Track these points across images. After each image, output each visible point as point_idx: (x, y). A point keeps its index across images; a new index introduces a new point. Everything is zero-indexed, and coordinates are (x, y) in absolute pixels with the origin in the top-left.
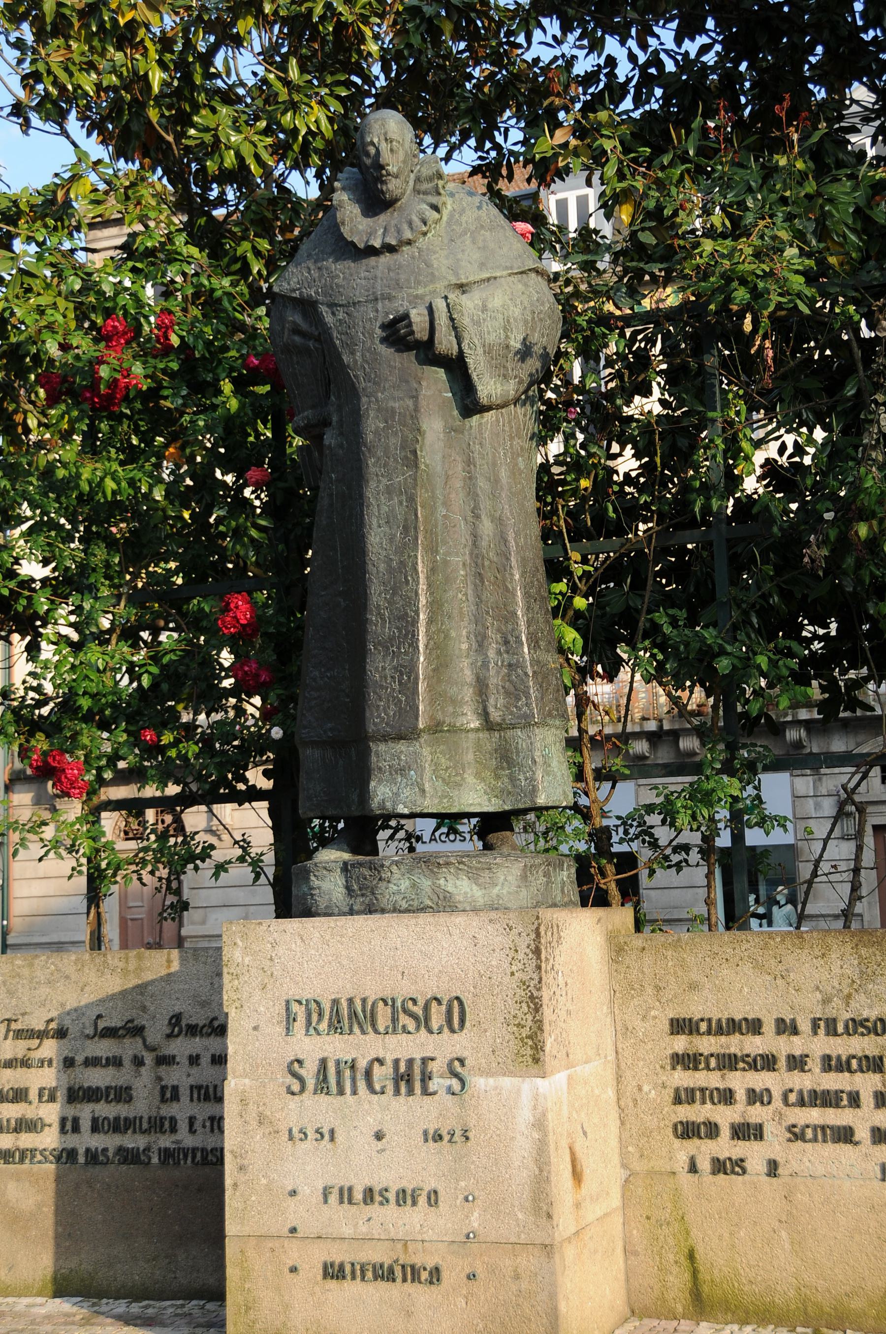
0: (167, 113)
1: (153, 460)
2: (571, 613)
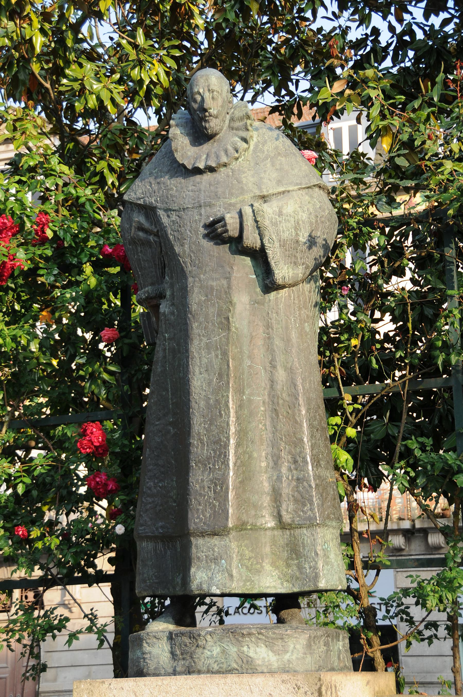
0: (46, 67)
1: (31, 321)
2: (344, 440)
